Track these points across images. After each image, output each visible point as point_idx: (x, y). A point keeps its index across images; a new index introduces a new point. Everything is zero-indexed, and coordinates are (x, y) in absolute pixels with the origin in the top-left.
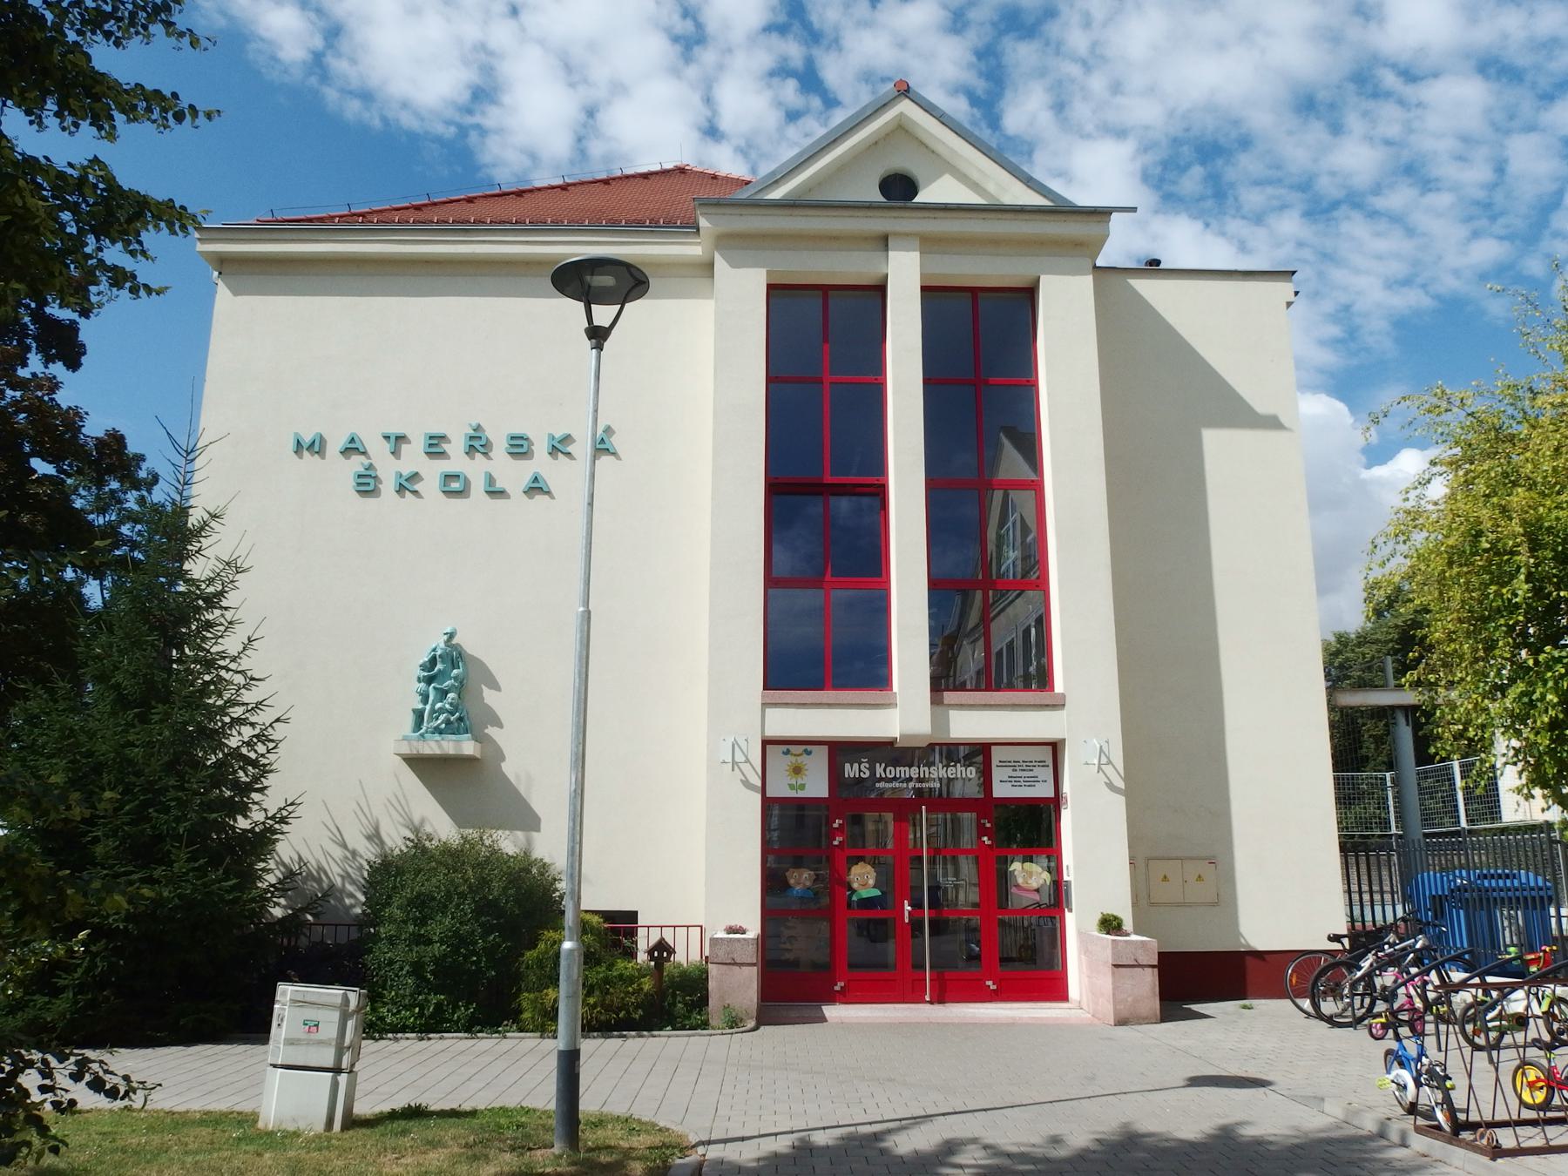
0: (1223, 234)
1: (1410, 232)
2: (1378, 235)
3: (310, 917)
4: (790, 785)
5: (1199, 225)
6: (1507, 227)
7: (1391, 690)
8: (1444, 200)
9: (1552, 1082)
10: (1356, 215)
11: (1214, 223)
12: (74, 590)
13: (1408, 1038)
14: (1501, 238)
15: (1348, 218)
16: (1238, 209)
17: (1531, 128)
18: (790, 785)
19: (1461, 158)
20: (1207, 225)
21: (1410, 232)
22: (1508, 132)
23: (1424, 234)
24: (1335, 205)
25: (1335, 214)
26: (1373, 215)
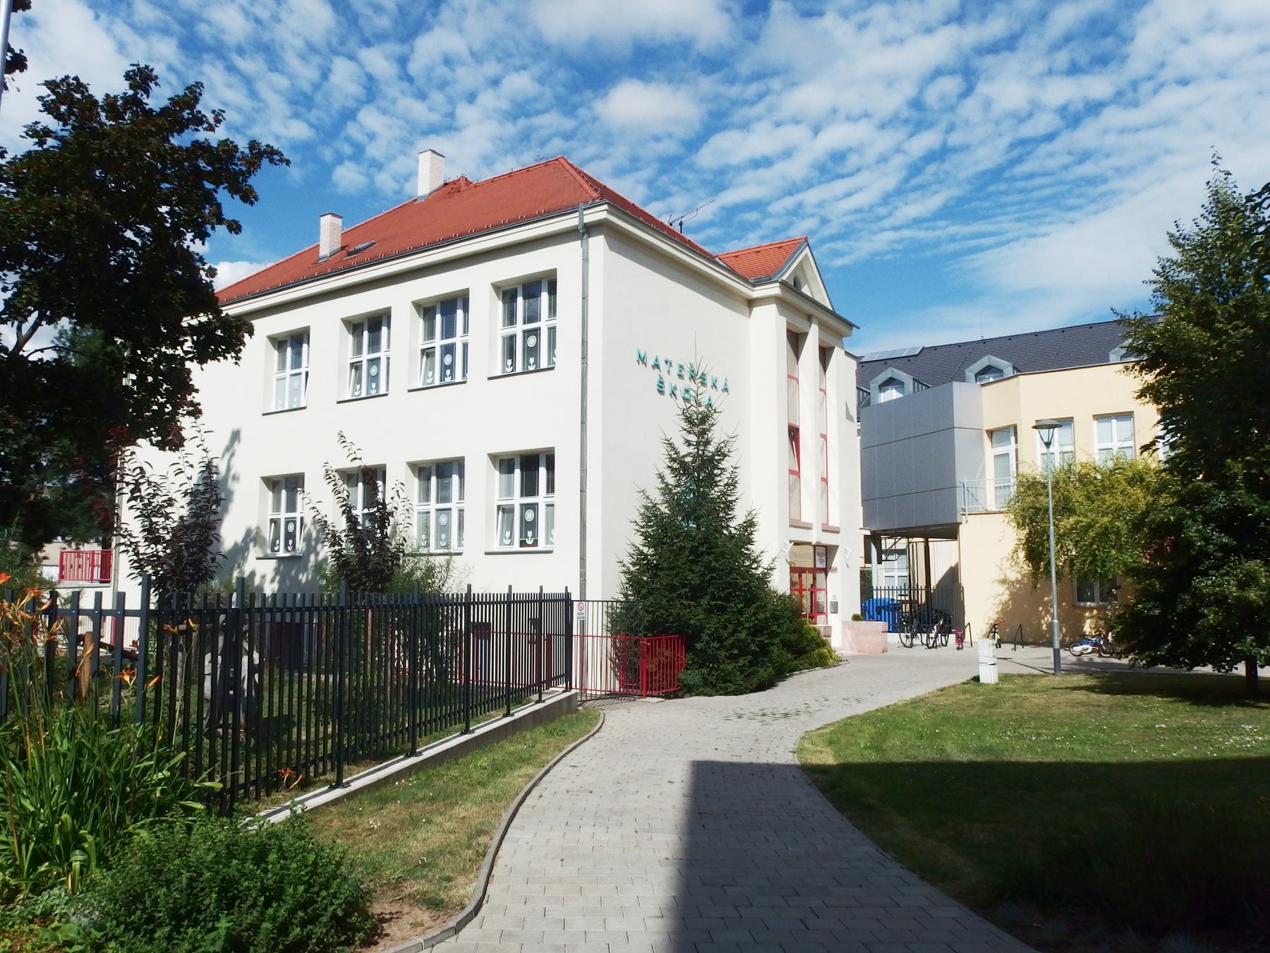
0: (108, 31)
1: (253, 94)
2: (230, 86)
3: (145, 206)
4: (39, 123)
5: (90, 14)
6: (319, 118)
7: (459, 297)
8: (283, 82)
9: (1268, 723)
10: (220, 64)
11: (104, 17)
12: (152, 356)
13: (895, 543)
14: (312, 126)
15: (212, 64)
16: (130, 15)
17: (352, 57)
18: (39, 123)
19: (303, 57)
20: (97, 17)
21: (253, 94)
22: (336, 53)
23: (262, 101)
24: (208, 49)
25: (205, 56)
26: (231, 69)
